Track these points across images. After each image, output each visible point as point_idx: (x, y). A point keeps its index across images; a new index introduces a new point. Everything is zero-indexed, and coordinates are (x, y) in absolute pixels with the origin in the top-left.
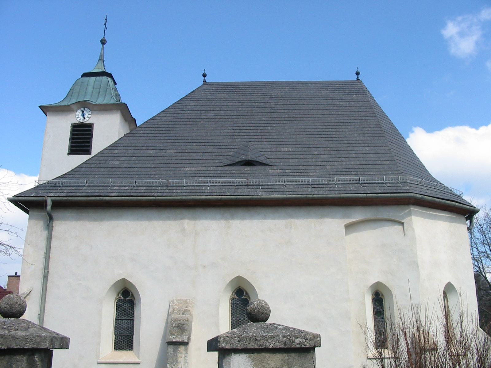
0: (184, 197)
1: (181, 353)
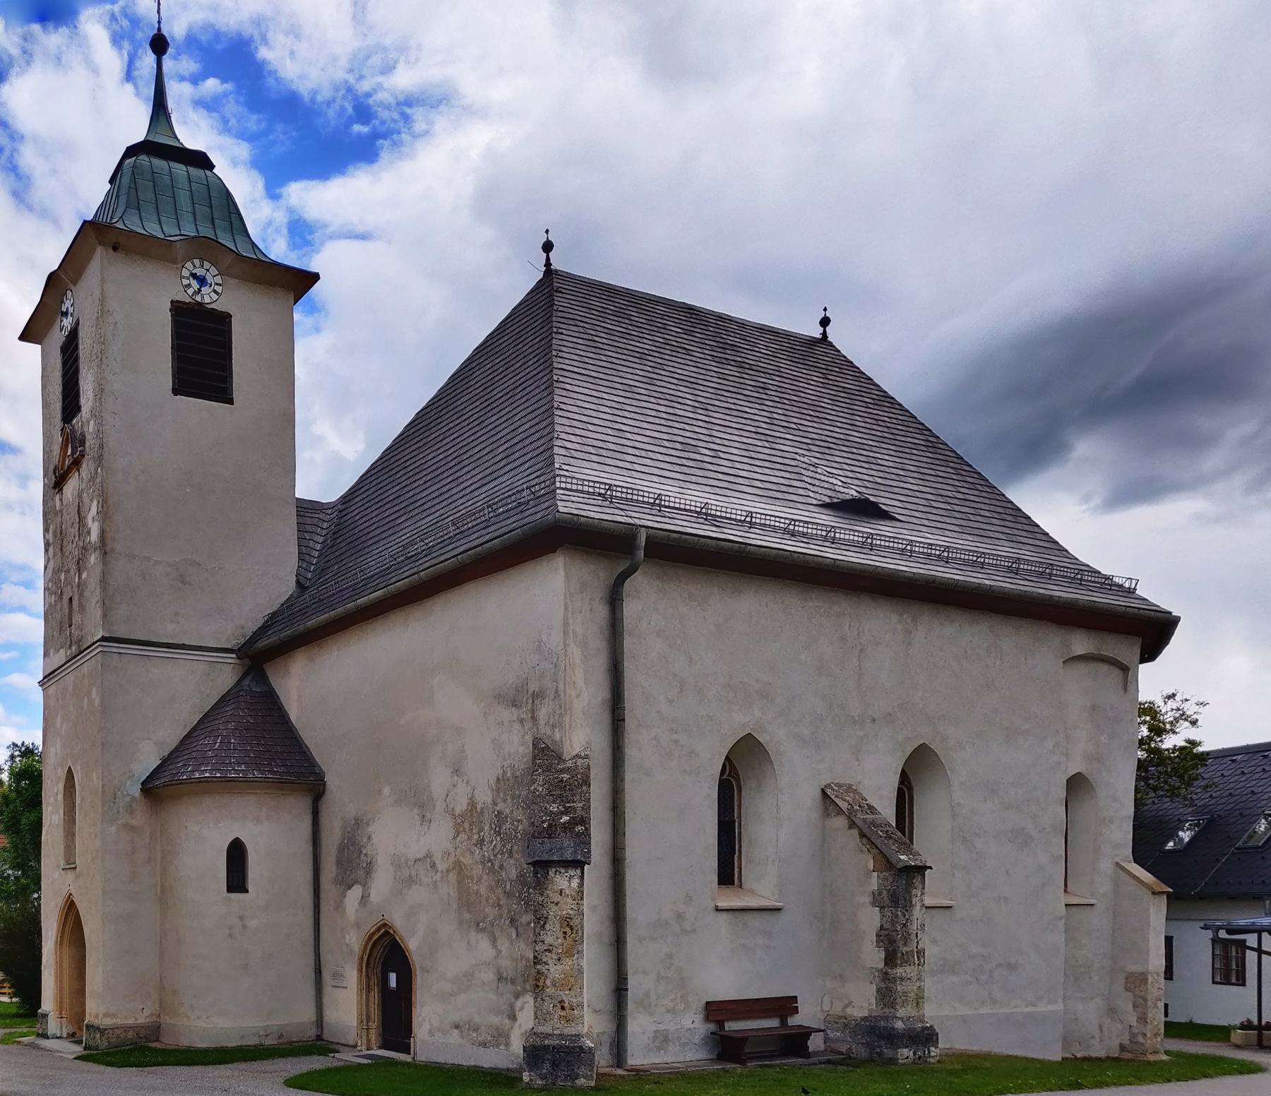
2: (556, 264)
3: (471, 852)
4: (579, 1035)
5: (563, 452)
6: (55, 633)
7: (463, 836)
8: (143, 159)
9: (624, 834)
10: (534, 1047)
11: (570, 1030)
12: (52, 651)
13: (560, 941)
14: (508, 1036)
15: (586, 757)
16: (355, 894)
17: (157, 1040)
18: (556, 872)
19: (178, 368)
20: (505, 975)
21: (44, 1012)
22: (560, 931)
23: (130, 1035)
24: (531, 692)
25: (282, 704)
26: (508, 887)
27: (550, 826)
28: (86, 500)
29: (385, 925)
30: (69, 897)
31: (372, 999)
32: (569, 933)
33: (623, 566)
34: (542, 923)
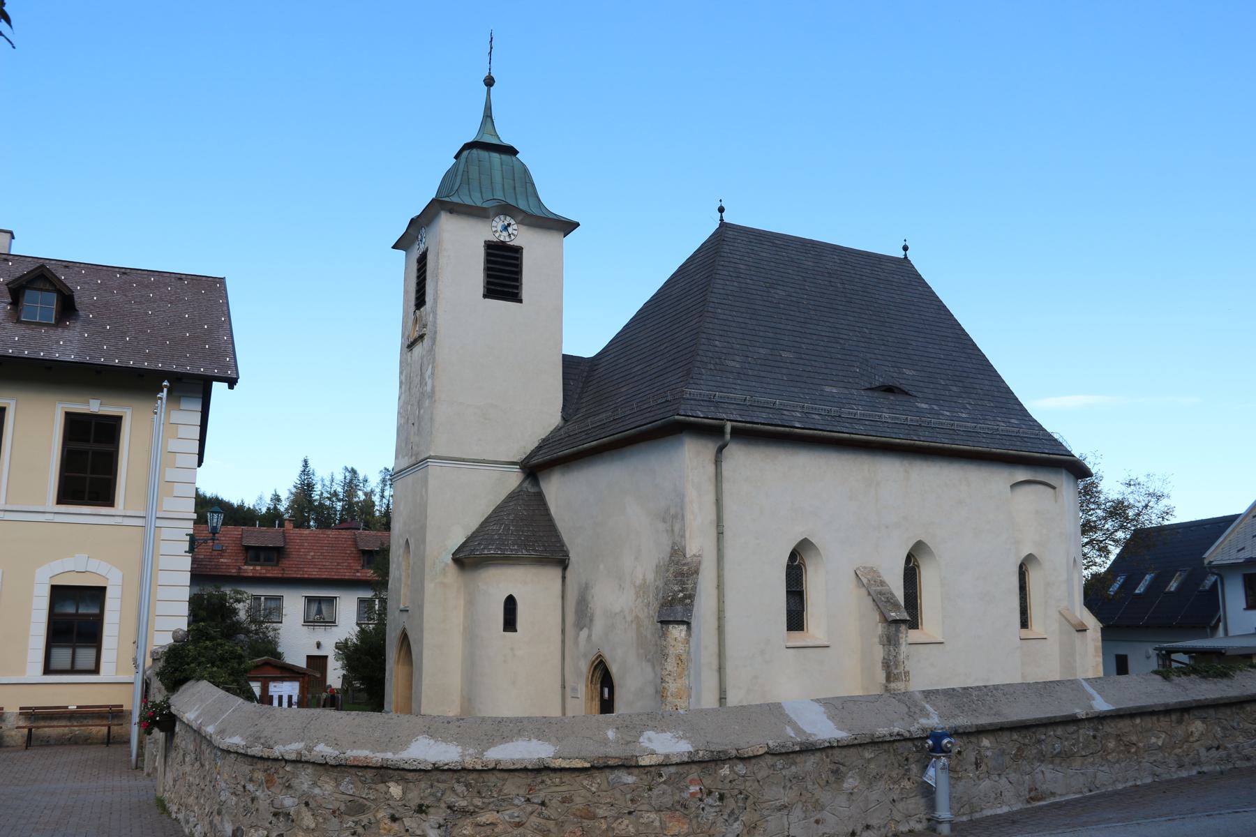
0: (879, 438)
1: (902, 633)
2: (726, 220)
7: (640, 600)
8: (474, 151)
12: (400, 456)
15: (699, 556)
16: (584, 634)
19: (488, 274)
27: (672, 599)
30: (404, 631)
31: (593, 706)
33: (720, 443)
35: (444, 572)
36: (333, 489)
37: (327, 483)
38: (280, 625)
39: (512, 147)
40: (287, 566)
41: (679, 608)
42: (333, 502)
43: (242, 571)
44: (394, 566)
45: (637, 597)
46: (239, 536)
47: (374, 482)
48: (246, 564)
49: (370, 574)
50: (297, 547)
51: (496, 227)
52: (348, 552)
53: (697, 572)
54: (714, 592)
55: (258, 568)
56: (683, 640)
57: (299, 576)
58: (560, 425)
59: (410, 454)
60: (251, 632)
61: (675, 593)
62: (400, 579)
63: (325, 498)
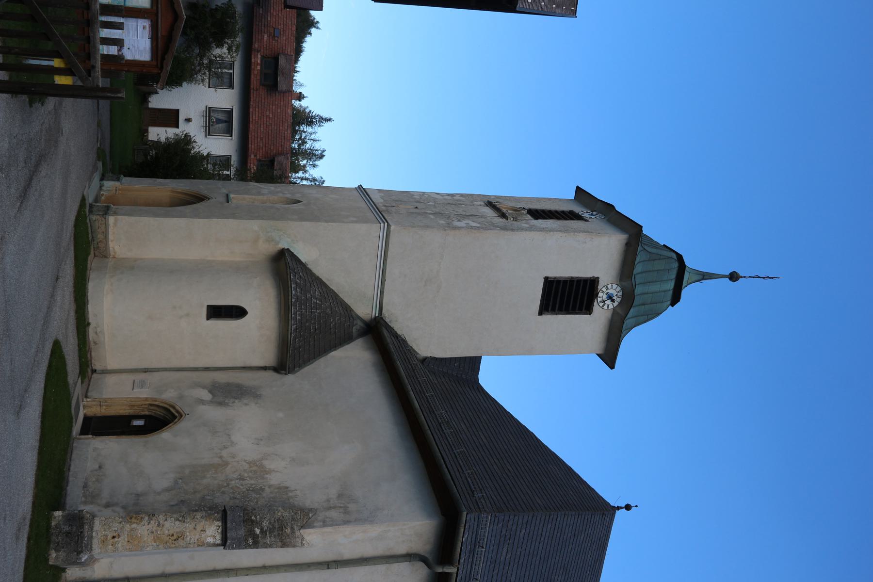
3: (235, 472)
4: (92, 550)
5: (507, 518)
6: (394, 197)
7: (246, 466)
8: (676, 265)
9: (247, 575)
10: (83, 518)
11: (96, 544)
13: (167, 532)
14: (92, 503)
15: (302, 545)
16: (205, 395)
17: (95, 256)
18: (219, 526)
19: (560, 281)
20: (141, 498)
21: (121, 179)
22: (174, 532)
23: (100, 236)
24: (349, 505)
25: (343, 346)
26: (209, 498)
27: (252, 521)
28: (480, 220)
29: (181, 416)
30: (207, 198)
32: (173, 538)
33: (430, 558)
34: (180, 519)
35: (269, 240)
36: (307, 140)
37: (313, 137)
38: (207, 86)
39: (679, 301)
40: (260, 93)
41: (242, 532)
42: (298, 141)
43: (256, 53)
44: (273, 188)
45: (249, 463)
46: (286, 52)
47: (313, 172)
48: (262, 57)
49: (253, 167)
50: (277, 103)
51: (612, 288)
52: (272, 147)
53: (284, 545)
54: (259, 562)
55: (259, 68)
56: (202, 539)
57: (251, 103)
58: (418, 356)
59: (387, 205)
60: (201, 59)
61: (258, 524)
62: (259, 193)
63: (301, 134)
